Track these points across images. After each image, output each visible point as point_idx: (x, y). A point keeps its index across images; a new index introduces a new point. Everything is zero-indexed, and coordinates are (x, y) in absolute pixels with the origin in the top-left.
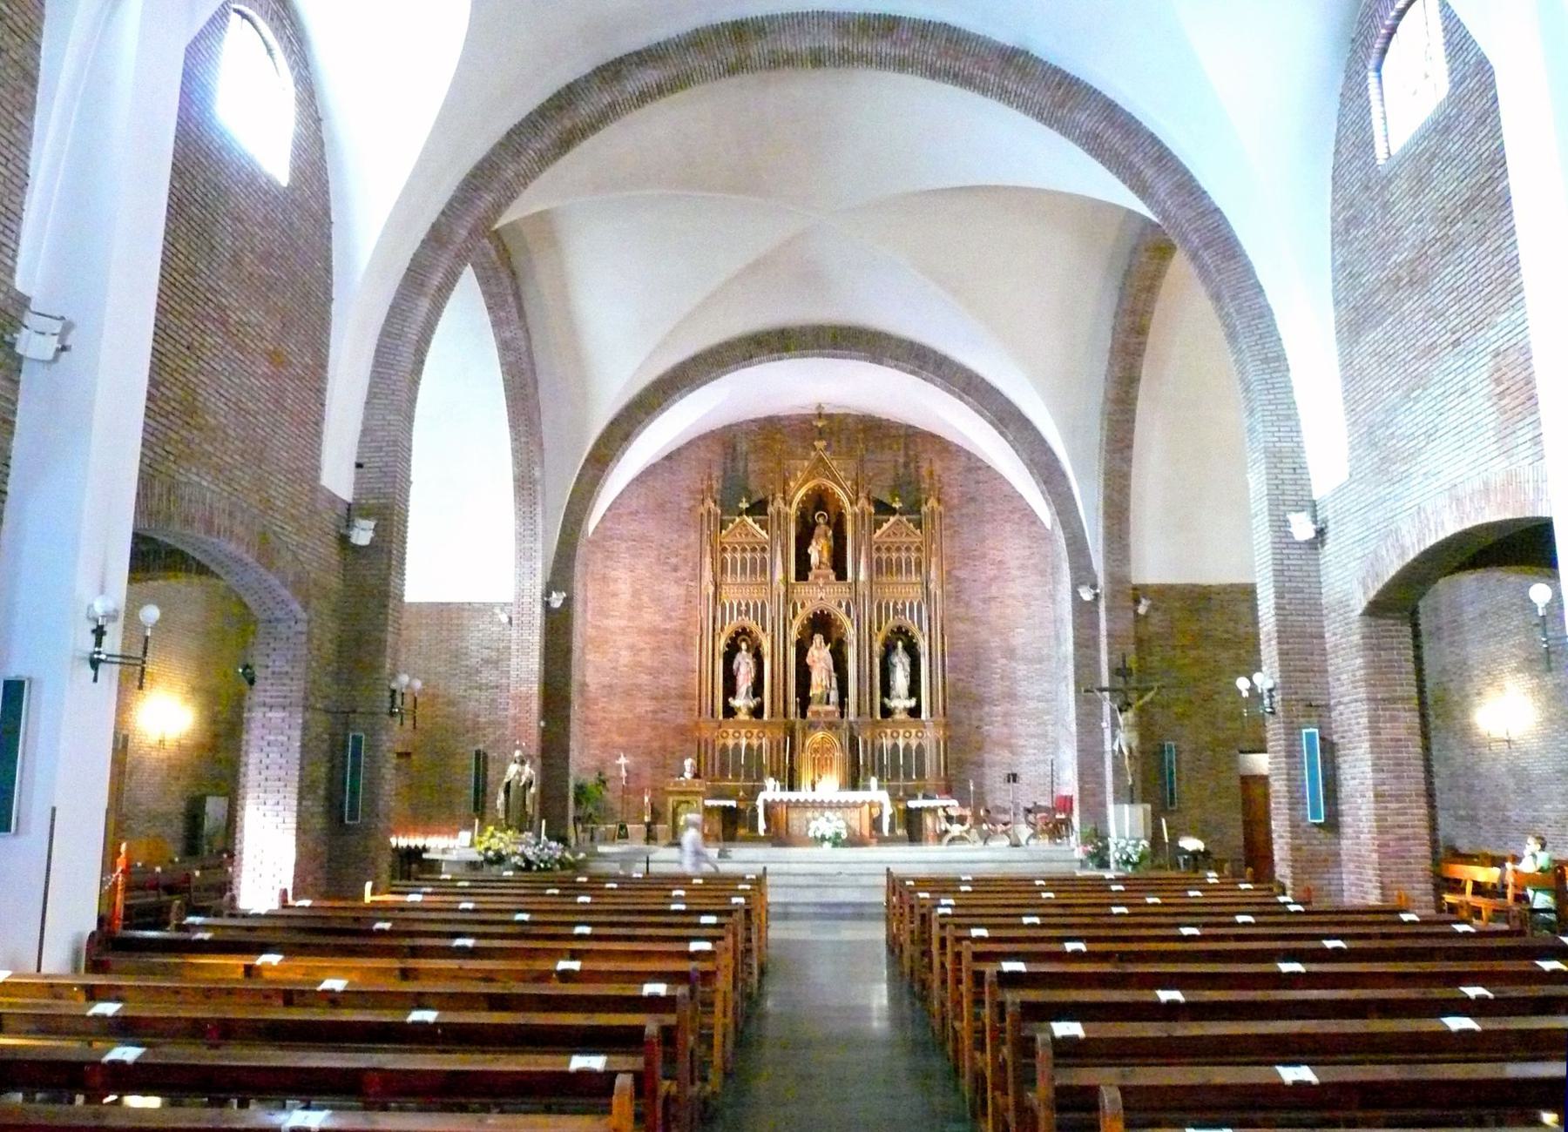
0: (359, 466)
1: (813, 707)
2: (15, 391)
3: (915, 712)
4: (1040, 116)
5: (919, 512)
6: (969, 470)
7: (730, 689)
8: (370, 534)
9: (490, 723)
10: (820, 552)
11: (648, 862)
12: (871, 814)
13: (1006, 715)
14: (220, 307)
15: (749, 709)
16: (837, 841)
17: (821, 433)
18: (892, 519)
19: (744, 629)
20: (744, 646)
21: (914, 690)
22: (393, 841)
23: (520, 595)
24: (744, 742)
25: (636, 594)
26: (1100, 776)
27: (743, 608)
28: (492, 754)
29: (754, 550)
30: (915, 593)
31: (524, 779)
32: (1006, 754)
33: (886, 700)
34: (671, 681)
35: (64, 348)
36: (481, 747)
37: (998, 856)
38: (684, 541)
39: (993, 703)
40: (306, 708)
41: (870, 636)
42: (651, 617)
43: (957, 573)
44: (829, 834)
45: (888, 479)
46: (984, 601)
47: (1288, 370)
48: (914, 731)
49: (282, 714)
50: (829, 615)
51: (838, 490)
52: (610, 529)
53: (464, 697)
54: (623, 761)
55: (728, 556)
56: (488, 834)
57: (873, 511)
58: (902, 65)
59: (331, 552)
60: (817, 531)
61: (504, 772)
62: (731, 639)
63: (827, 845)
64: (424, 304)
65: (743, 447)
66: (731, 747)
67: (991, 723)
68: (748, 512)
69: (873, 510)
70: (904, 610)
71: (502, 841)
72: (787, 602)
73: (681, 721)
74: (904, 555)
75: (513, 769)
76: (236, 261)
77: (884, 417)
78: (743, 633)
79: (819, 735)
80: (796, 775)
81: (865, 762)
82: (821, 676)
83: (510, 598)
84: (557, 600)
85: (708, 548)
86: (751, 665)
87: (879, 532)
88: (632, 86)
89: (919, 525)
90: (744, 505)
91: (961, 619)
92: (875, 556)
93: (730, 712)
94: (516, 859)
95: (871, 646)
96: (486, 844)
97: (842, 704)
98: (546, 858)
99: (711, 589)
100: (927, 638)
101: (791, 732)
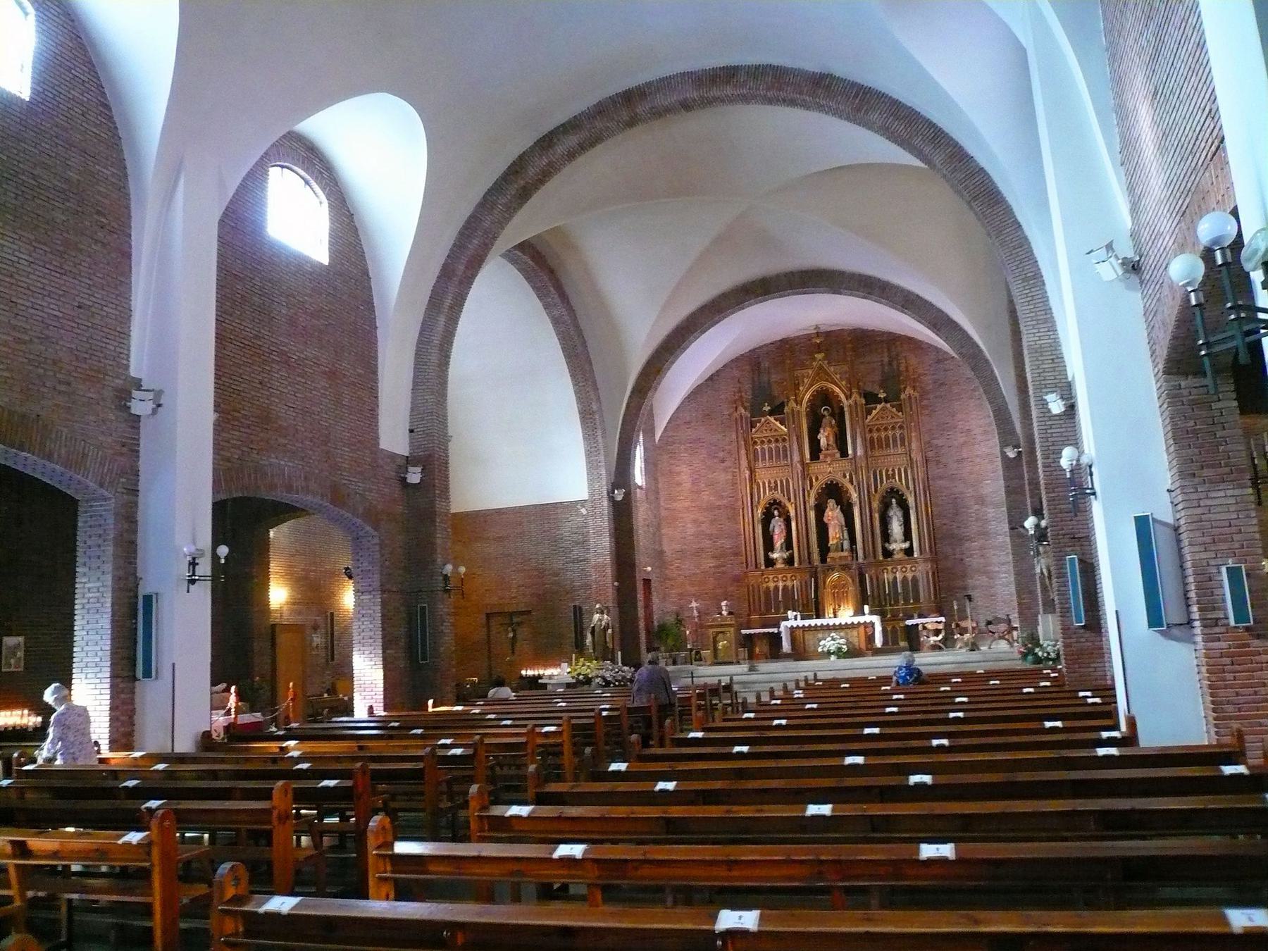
0: (411, 431)
1: (831, 555)
2: (138, 434)
3: (909, 552)
4: (848, 119)
5: (899, 399)
6: (939, 361)
7: (769, 546)
8: (419, 476)
9: (581, 587)
10: (827, 437)
11: (692, 677)
12: (866, 632)
13: (981, 548)
14: (283, 353)
15: (784, 559)
16: (839, 653)
17: (819, 348)
18: (879, 407)
19: (775, 500)
20: (776, 513)
21: (907, 535)
22: (523, 672)
23: (592, 494)
24: (781, 584)
25: (695, 482)
26: (1032, 593)
27: (773, 485)
28: (585, 608)
29: (777, 441)
30: (903, 460)
31: (603, 623)
32: (985, 579)
33: (887, 545)
34: (728, 544)
35: (159, 405)
36: (577, 603)
37: (959, 658)
38: (728, 439)
39: (970, 540)
40: (383, 592)
41: (869, 498)
42: (707, 497)
43: (935, 442)
44: (833, 649)
45: (877, 377)
46: (959, 461)
47: (1044, 284)
48: (789, 576)
49: (369, 597)
50: (837, 484)
51: (837, 390)
52: (671, 437)
53: (563, 569)
54: (694, 604)
55: (758, 447)
56: (581, 664)
57: (864, 402)
58: (746, 99)
59: (397, 492)
60: (824, 420)
61: (591, 620)
62: (766, 508)
63: (833, 658)
64: (442, 320)
65: (766, 364)
66: (910, 578)
67: (971, 556)
68: (771, 413)
69: (863, 401)
70: (894, 475)
71: (588, 668)
72: (804, 479)
73: (737, 572)
74: (890, 433)
75: (597, 616)
76: (292, 322)
77: (870, 328)
78: (775, 504)
79: (836, 575)
80: (821, 607)
81: (872, 592)
82: (835, 533)
83: (586, 497)
84: (619, 495)
85: (743, 443)
86: (783, 527)
87: (869, 417)
88: (560, 149)
89: (900, 409)
90: (767, 408)
91: (941, 478)
92: (868, 436)
93: (770, 563)
94: (598, 680)
95: (870, 504)
96: (579, 671)
97: (853, 550)
98: (620, 678)
99: (747, 473)
100: (913, 495)
101: (814, 574)
